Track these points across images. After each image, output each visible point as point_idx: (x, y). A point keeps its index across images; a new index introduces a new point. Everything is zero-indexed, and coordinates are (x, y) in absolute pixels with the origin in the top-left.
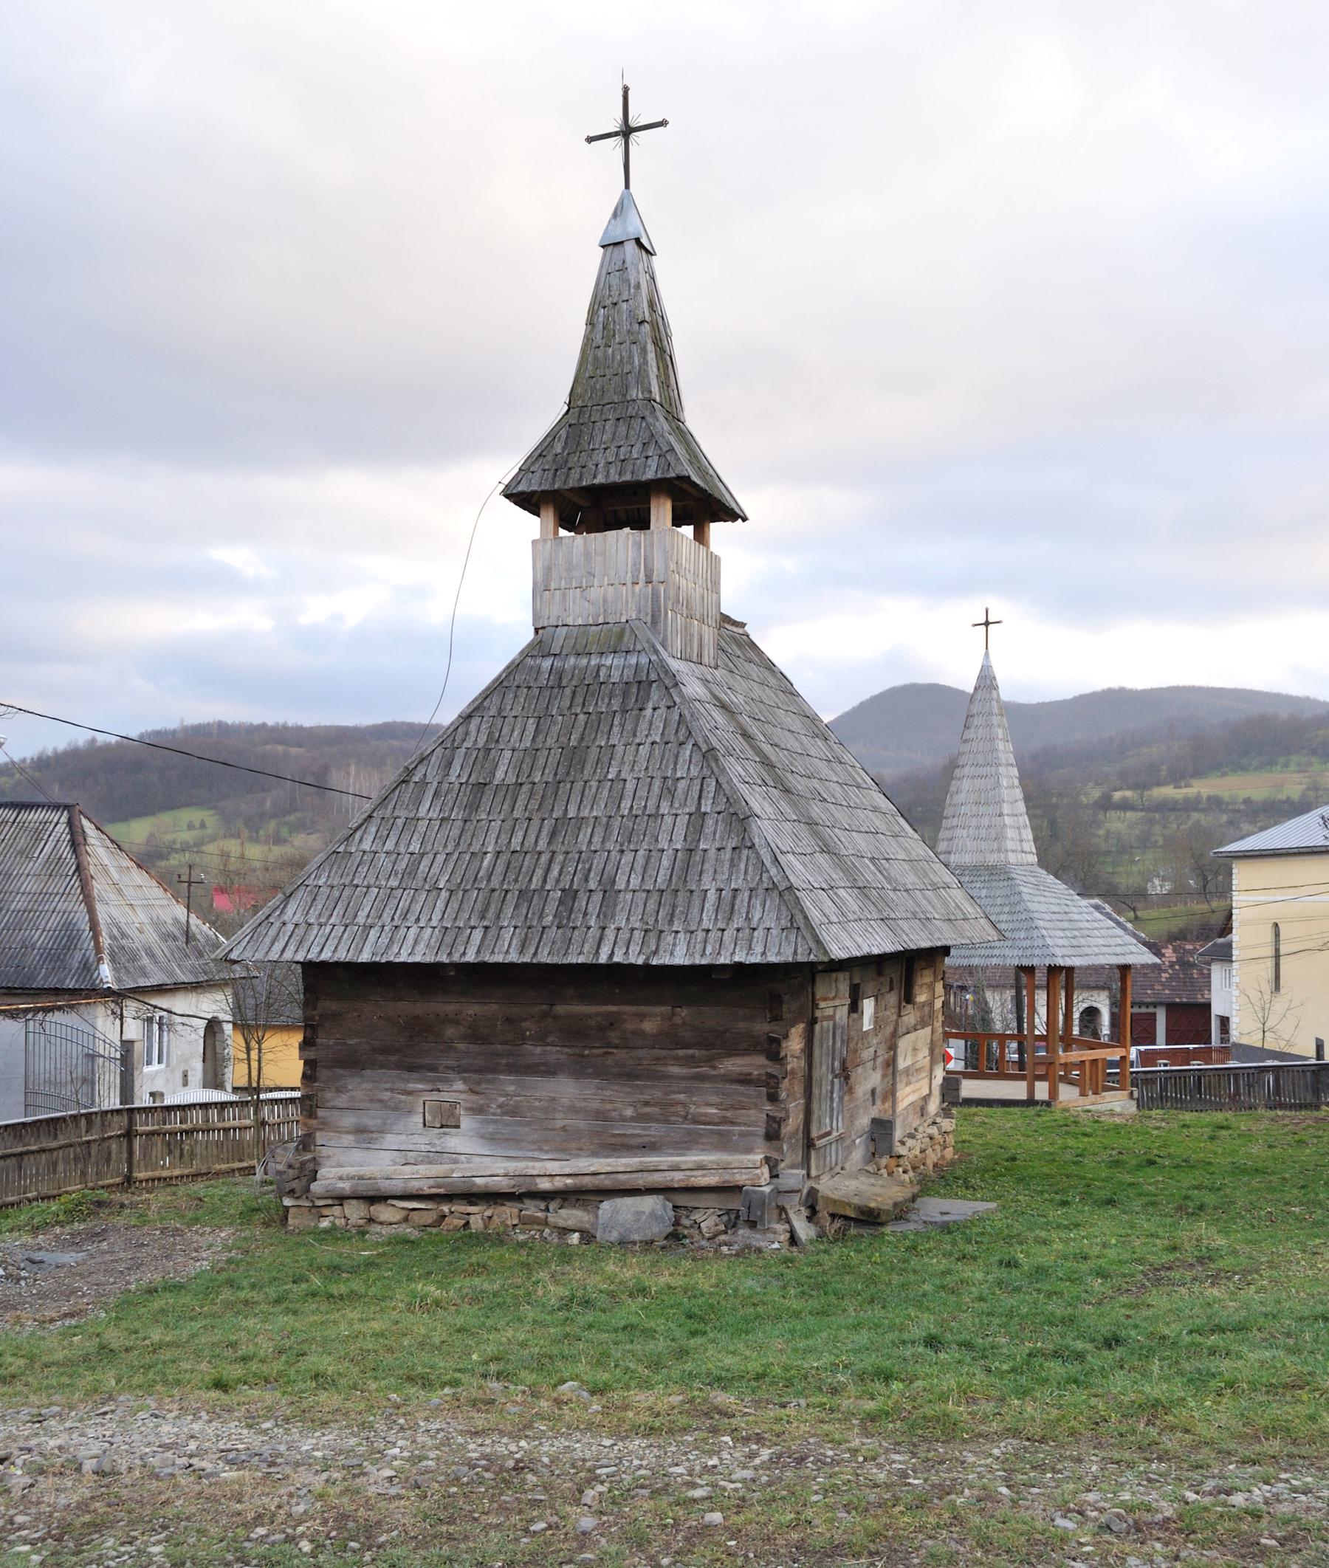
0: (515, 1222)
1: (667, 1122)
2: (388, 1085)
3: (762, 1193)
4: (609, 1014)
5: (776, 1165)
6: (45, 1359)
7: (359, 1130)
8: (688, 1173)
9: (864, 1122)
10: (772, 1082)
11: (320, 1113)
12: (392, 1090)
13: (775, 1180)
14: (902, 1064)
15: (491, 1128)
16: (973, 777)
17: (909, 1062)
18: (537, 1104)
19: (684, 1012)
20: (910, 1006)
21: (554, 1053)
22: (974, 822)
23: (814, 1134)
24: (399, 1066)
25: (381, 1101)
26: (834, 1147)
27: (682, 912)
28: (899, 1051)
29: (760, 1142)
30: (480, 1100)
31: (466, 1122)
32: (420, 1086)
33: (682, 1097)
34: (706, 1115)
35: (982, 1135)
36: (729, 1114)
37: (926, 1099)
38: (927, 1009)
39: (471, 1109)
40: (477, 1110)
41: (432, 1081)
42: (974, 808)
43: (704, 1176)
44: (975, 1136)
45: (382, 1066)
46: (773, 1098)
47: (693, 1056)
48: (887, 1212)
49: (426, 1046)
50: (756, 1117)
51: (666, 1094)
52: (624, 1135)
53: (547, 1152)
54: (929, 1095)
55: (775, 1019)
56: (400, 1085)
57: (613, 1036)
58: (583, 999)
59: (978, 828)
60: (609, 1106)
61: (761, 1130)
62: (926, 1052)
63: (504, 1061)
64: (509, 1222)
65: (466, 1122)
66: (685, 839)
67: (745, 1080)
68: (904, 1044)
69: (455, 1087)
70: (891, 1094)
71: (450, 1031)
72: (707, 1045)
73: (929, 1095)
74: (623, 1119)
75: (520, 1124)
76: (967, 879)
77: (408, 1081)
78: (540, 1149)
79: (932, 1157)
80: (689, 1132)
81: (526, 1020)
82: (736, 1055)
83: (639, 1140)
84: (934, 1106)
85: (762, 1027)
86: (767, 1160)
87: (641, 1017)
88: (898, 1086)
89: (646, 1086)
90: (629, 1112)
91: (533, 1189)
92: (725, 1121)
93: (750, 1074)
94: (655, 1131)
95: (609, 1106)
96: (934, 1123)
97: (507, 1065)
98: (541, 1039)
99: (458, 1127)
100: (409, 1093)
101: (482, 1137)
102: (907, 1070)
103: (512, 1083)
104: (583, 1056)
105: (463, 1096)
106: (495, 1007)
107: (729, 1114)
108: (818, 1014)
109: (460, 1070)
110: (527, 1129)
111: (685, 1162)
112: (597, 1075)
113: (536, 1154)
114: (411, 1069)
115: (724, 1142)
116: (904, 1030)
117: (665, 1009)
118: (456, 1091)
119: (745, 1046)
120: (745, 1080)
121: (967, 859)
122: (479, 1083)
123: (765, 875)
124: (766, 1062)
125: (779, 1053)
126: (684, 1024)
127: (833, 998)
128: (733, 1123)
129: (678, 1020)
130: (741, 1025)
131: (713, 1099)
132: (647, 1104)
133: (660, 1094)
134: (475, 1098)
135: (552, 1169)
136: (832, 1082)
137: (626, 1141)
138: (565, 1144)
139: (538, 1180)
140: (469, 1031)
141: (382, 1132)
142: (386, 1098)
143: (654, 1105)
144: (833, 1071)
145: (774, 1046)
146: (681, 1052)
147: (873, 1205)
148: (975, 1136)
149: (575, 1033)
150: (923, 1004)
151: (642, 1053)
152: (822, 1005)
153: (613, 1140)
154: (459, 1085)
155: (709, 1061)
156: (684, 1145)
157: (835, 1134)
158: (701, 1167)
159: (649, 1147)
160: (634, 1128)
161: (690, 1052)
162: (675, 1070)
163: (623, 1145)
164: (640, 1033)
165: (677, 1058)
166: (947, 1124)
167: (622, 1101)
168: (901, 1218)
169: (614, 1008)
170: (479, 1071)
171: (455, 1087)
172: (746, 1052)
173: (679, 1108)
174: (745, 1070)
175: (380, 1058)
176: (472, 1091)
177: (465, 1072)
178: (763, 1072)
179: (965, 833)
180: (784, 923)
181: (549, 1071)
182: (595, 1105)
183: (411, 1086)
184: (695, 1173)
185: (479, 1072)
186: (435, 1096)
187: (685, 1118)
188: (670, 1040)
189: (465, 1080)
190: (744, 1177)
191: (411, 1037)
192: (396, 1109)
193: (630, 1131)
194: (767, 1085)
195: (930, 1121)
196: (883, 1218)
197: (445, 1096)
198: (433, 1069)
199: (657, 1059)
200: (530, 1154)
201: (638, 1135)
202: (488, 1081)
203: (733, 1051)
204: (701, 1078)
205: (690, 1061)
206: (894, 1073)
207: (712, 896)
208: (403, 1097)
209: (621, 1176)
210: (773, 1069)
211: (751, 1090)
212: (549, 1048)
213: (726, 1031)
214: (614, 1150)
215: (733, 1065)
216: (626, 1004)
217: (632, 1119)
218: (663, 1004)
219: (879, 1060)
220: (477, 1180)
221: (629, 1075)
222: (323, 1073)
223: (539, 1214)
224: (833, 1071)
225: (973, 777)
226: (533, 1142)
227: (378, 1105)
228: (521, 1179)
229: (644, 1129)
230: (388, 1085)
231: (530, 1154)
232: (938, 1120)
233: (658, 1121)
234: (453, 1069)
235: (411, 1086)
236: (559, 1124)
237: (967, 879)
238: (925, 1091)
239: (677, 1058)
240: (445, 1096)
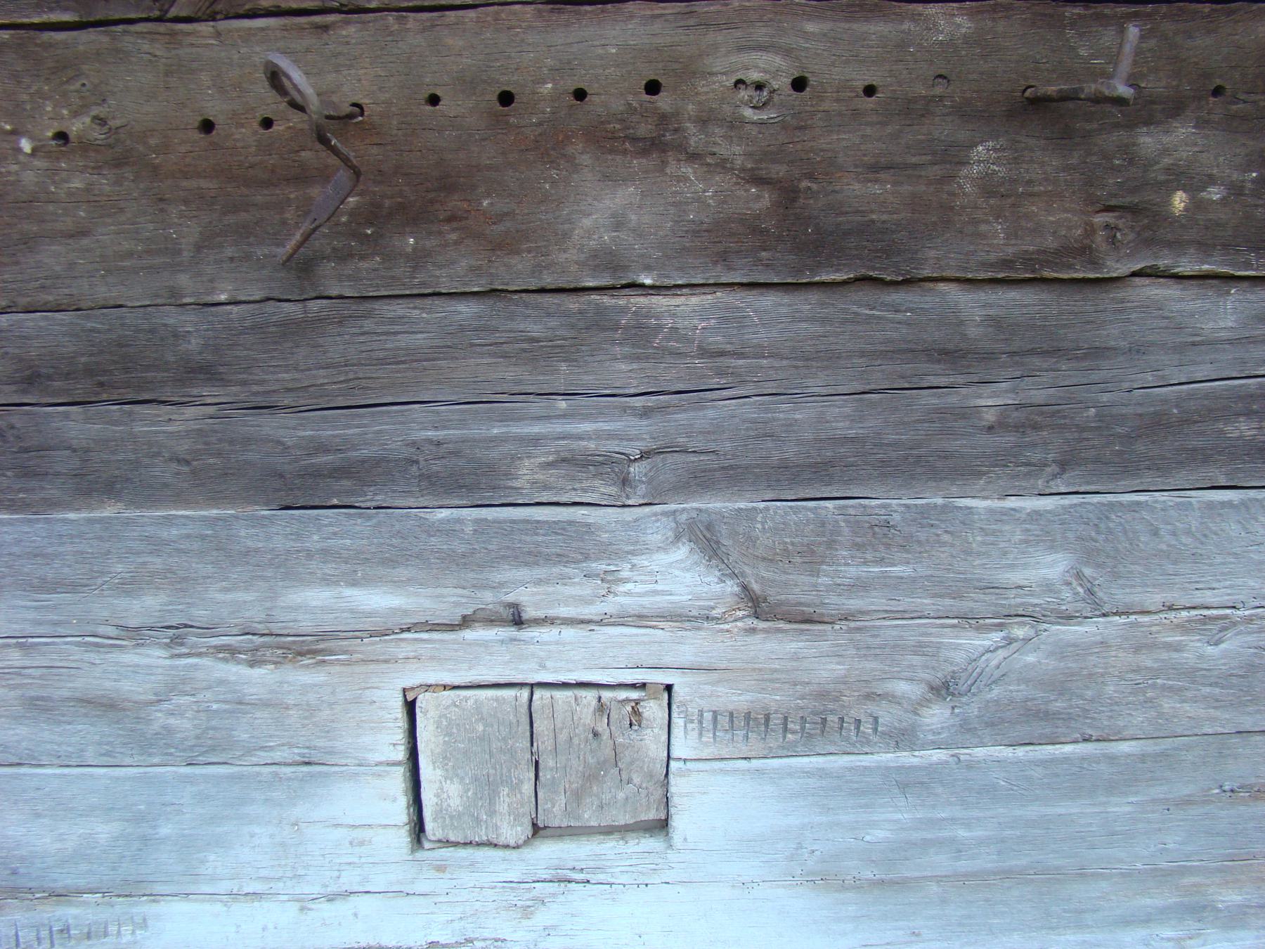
2: (146, 606)
6: (186, 469)
12: (176, 635)
15: (888, 822)
18: (1198, 650)
24: (215, 474)
25: (106, 706)
30: (818, 659)
31: (719, 800)
32: (377, 600)
39: (755, 722)
41: (460, 561)
45: (94, 482)
49: (421, 324)
56: (231, 600)
63: (990, 401)
65: (719, 800)
69: (633, 592)
71: (607, 210)
75: (1077, 780)
77: (287, 568)
100: (306, 648)
101: (826, 878)
103: (1043, 533)
105: (691, 646)
106: (163, 597)
110: (1120, 807)
114: (307, 486)
118: (643, 601)
122: (812, 557)
134: (777, 647)
140: (760, 201)
141: (133, 889)
142: (130, 687)
154: (672, 573)
171: (633, 592)
175: (76, 426)
176: (758, 606)
177: (700, 481)
183: (313, 602)
185: (780, 482)
186: (491, 655)
189: (707, 541)
191: (302, 267)
192: (206, 748)
197: (556, 654)
198: (472, 479)
202: (879, 537)
208: (258, 679)
227: (86, 732)
230: (146, 606)
234: (612, 468)
235: (313, 602)
240: (556, 654)
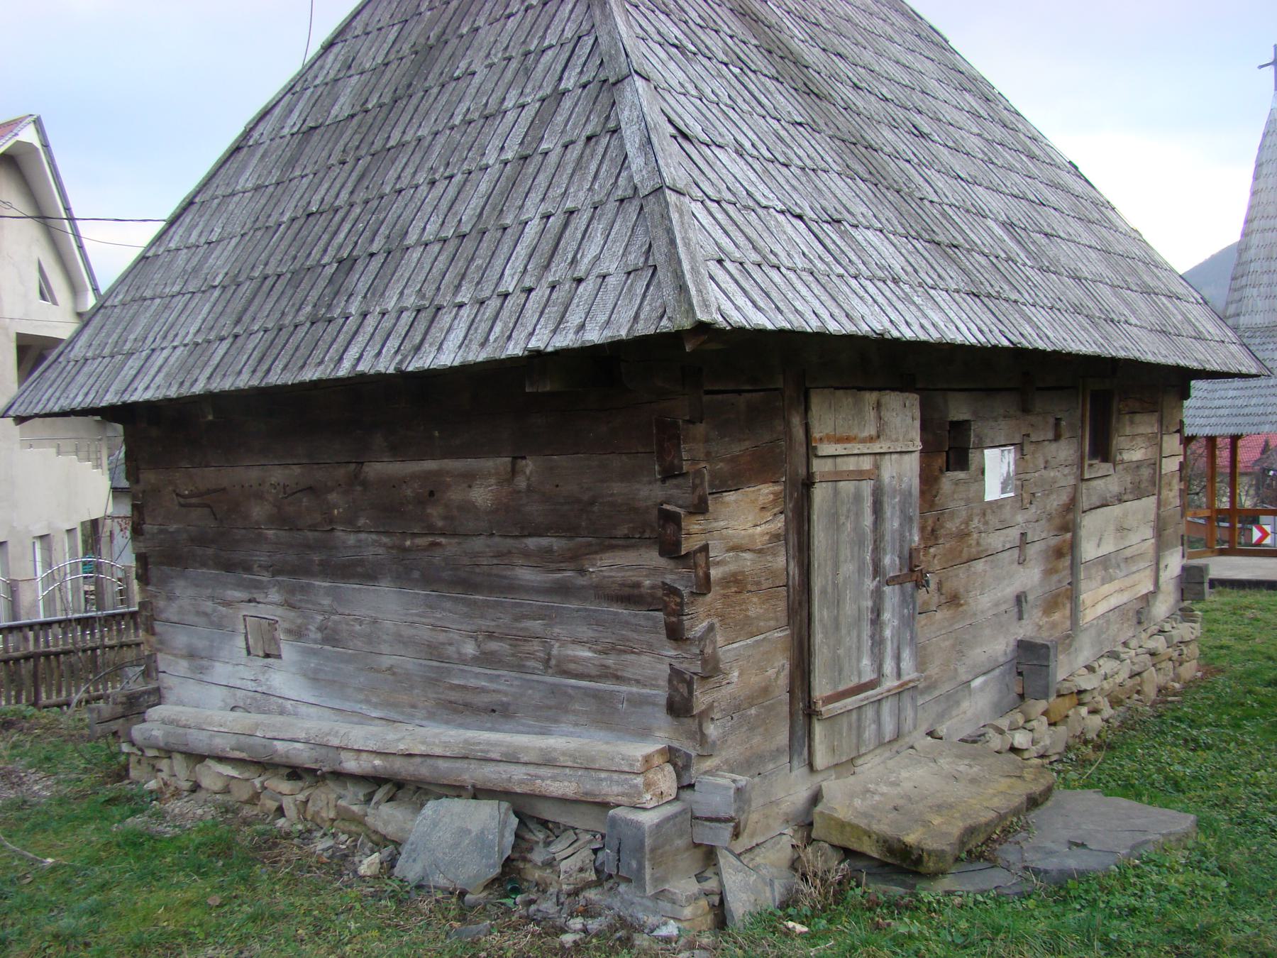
0: (332, 815)
1: (521, 668)
3: (638, 826)
4: (426, 476)
5: (687, 767)
7: (192, 655)
8: (532, 770)
9: (999, 647)
10: (673, 602)
11: (158, 627)
13: (686, 795)
14: (1089, 550)
16: (1263, 231)
17: (1108, 547)
19: (529, 465)
20: (1105, 468)
21: (365, 543)
22: (1265, 279)
23: (821, 688)
26: (886, 707)
27: (479, 267)
28: (1083, 533)
29: (662, 719)
31: (288, 650)
33: (536, 625)
34: (575, 660)
35: (1249, 637)
36: (610, 661)
37: (1147, 599)
38: (1146, 472)
40: (297, 634)
42: (1266, 264)
43: (554, 778)
44: (1239, 638)
46: (675, 634)
47: (549, 550)
48: (940, 855)
50: (653, 665)
51: (517, 619)
52: (464, 688)
53: (375, 706)
54: (1154, 593)
55: (670, 474)
57: (435, 513)
58: (398, 451)
59: (1270, 285)
60: (442, 637)
61: (661, 695)
62: (1148, 532)
64: (324, 814)
65: (288, 650)
66: (522, 143)
67: (630, 596)
68: (1090, 523)
70: (1066, 597)
72: (569, 530)
73: (1154, 593)
74: (463, 660)
76: (1257, 341)
78: (368, 702)
79: (1153, 680)
80: (554, 690)
81: (331, 490)
82: (612, 548)
83: (484, 699)
84: (1163, 607)
85: (650, 492)
86: (671, 755)
87: (469, 478)
88: (1083, 585)
89: (487, 604)
90: (470, 649)
91: (337, 768)
92: (606, 674)
93: (637, 585)
94: (504, 684)
95: (442, 637)
96: (1161, 631)
97: (322, 563)
98: (350, 522)
99: (279, 657)
100: (228, 604)
102: (1104, 562)
104: (406, 550)
107: (610, 661)
108: (818, 466)
109: (276, 570)
110: (351, 668)
111: (526, 749)
112: (429, 580)
113: (365, 709)
114: (229, 567)
115: (605, 713)
116: (1095, 501)
117: (504, 462)
118: (271, 605)
119: (623, 530)
120: (630, 596)
121: (1259, 320)
123: (624, 174)
124: (662, 562)
125: (678, 544)
126: (530, 490)
127: (871, 439)
128: (618, 679)
129: (521, 483)
130: (618, 489)
131: (585, 632)
132: (490, 636)
133: (506, 619)
134: (292, 614)
135: (366, 737)
136: (878, 595)
137: (469, 697)
138: (396, 693)
139: (343, 755)
143: (501, 639)
144: (877, 570)
145: (670, 529)
146: (532, 543)
147: (911, 839)
148: (1239, 638)
149: (392, 510)
150: (1138, 465)
151: (478, 544)
152: (826, 449)
153: (454, 696)
154: (274, 596)
155: (574, 558)
156: (552, 710)
157: (890, 683)
158: (547, 761)
159: (498, 712)
160: (477, 675)
161: (544, 542)
162: (527, 575)
163: (466, 705)
164: (468, 508)
165: (526, 554)
166: (1184, 630)
167: (458, 629)
168: (981, 856)
169: (430, 465)
170: (294, 571)
172: (628, 543)
173: (535, 646)
174: (632, 576)
178: (658, 581)
179: (1255, 292)
180: (635, 258)
181: (365, 573)
182: (425, 633)
184: (542, 771)
186: (250, 610)
187: (547, 662)
188: (512, 521)
190: (616, 789)
193: (473, 682)
194: (664, 608)
195: (1154, 628)
196: (931, 865)
199: (499, 555)
200: (357, 707)
201: (483, 690)
203: (609, 544)
204: (563, 590)
205: (545, 559)
206: (1074, 568)
207: (531, 231)
209: (442, 764)
210: (675, 577)
211: (637, 616)
212: (363, 536)
213: (592, 503)
214: (456, 711)
215: (614, 566)
216: (444, 456)
217: (476, 660)
218: (499, 455)
219: (1033, 551)
220: (280, 746)
221: (463, 582)
222: (154, 572)
223: (355, 808)
224: (877, 570)
225: (1263, 231)
226: (361, 690)
228: (324, 751)
229: (492, 679)
231: (357, 707)
232: (1167, 627)
233: (511, 667)
236: (386, 661)
237: (1257, 341)
238: (1146, 587)
239: (526, 554)
